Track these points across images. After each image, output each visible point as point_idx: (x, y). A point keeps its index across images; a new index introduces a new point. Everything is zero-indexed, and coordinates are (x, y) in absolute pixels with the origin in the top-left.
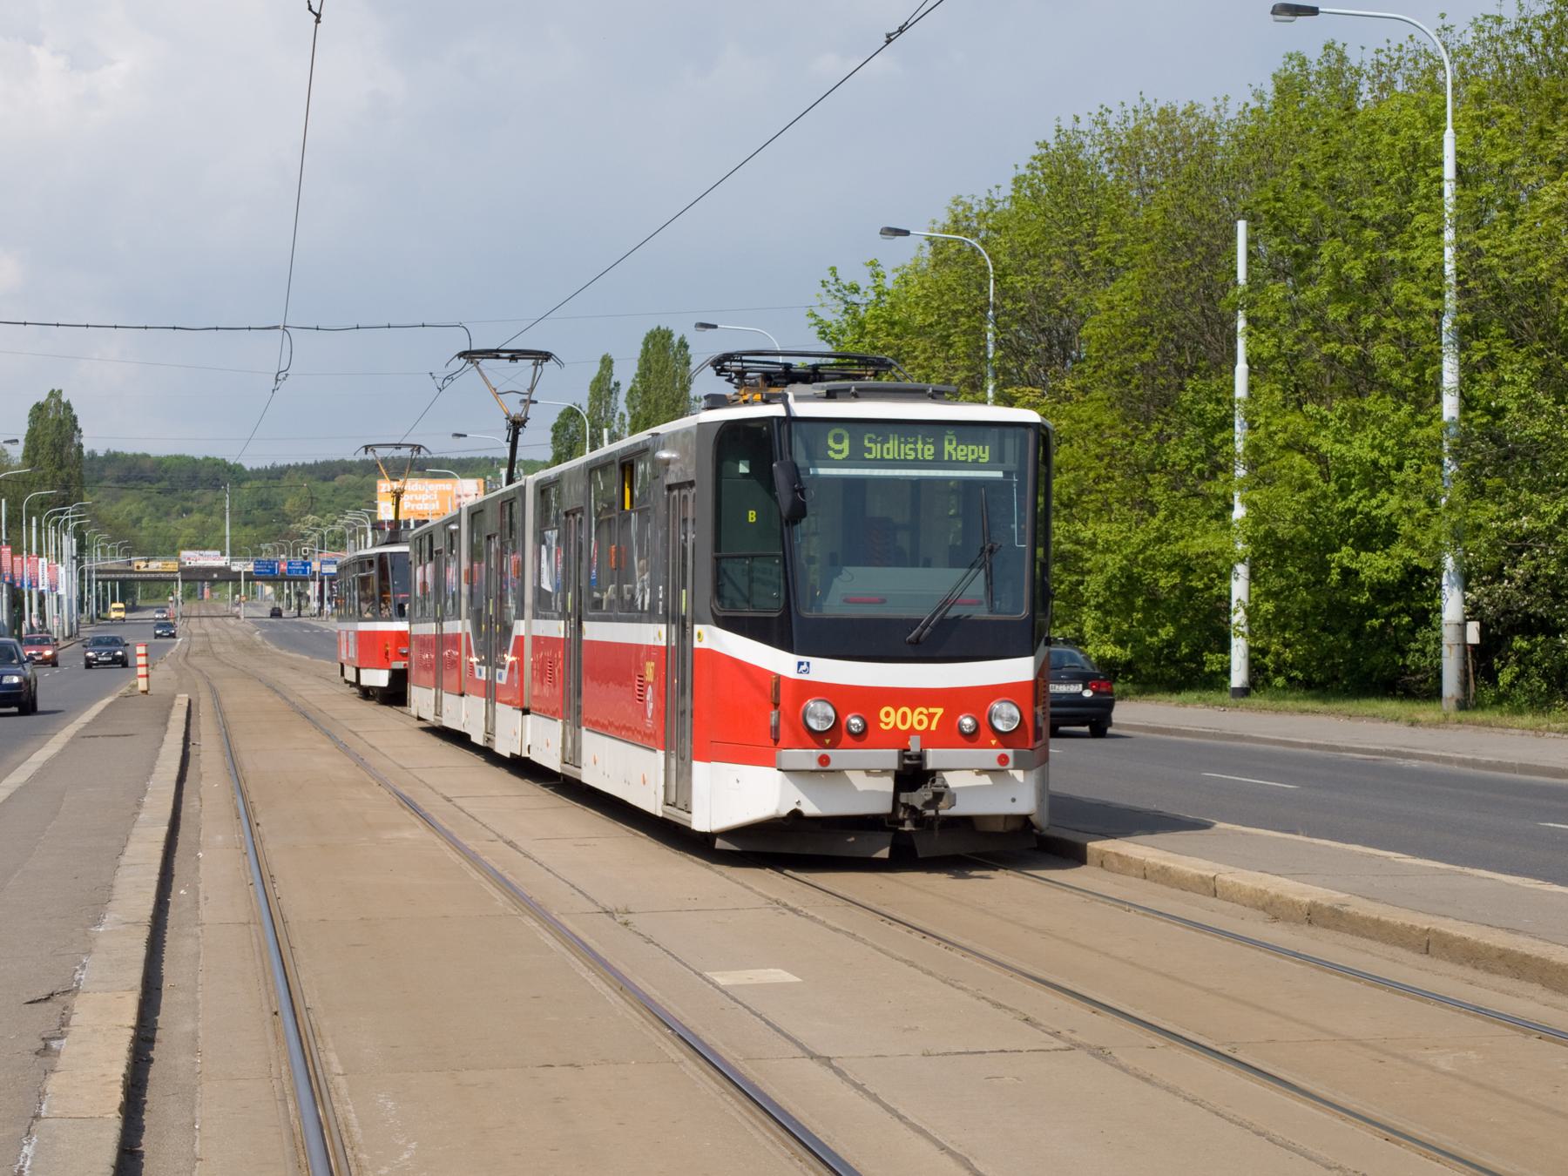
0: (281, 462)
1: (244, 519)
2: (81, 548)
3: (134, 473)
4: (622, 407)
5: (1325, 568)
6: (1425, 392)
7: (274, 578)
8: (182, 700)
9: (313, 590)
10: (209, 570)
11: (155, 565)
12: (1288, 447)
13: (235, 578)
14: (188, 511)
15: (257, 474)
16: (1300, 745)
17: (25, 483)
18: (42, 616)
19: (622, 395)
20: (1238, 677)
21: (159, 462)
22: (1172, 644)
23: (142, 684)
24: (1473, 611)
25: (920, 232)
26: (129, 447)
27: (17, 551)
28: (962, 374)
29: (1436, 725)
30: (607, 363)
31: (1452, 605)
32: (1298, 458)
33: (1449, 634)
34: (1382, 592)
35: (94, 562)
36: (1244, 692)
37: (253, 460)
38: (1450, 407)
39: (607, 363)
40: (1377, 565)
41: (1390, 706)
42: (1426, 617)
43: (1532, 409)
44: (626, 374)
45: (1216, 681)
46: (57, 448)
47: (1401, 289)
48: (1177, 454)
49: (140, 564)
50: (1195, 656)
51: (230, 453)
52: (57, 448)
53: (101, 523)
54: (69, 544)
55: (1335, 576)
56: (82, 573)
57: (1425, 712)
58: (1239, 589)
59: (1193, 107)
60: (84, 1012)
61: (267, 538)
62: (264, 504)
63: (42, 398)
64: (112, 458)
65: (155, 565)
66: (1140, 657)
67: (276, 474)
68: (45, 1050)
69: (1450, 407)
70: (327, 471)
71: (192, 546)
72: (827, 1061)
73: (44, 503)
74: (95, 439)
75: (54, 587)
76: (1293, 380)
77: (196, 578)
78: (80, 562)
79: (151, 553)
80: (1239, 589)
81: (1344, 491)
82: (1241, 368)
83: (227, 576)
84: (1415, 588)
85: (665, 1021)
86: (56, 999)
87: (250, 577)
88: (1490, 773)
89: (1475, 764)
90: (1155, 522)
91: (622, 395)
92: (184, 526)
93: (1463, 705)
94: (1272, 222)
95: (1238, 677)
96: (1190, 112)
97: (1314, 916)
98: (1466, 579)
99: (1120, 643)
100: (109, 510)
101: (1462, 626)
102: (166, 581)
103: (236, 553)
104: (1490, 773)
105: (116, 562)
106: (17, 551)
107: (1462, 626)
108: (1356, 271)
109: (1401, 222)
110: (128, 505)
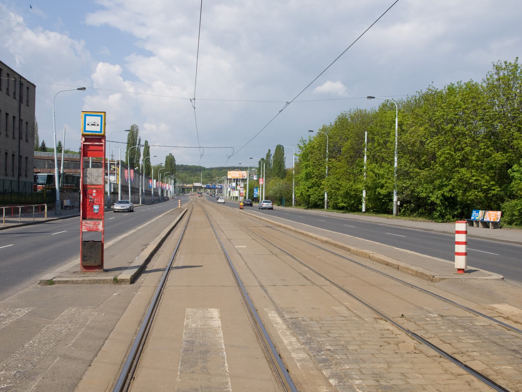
0: (212, 167)
1: (205, 177)
2: (175, 182)
3: (186, 168)
4: (272, 159)
5: (375, 192)
6: (392, 163)
7: (210, 189)
8: (186, 210)
9: (216, 191)
10: (198, 187)
11: (188, 185)
12: (370, 171)
13: (202, 188)
14: (195, 176)
15: (208, 169)
16: (407, 227)
17: (165, 171)
18: (167, 194)
19: (272, 156)
20: (364, 210)
21: (190, 166)
22: (353, 204)
23: (180, 206)
24: (398, 199)
25: (316, 131)
26: (185, 164)
27: (162, 183)
28: (322, 156)
29: (391, 218)
30: (269, 150)
31: (395, 198)
32: (371, 173)
33: (394, 203)
34: (385, 196)
35: (178, 184)
36: (365, 212)
37: (207, 167)
38: (396, 165)
39: (269, 150)
40: (383, 192)
41: (386, 215)
42: (391, 200)
43: (406, 166)
44: (273, 152)
45: (360, 210)
46: (171, 164)
47: (388, 145)
48: (355, 171)
49: (185, 185)
50: (357, 206)
51: (203, 166)
52: (171, 164)
53: (179, 178)
54: (173, 182)
55: (377, 193)
56: (175, 187)
57: (390, 216)
58: (364, 194)
59: (366, 110)
60: (149, 247)
61: (209, 181)
62: (209, 175)
63: (168, 155)
64: (182, 166)
65: (188, 185)
66: (349, 206)
67: (211, 169)
68: (143, 250)
69: (396, 165)
70: (220, 169)
71: (196, 182)
72: (240, 255)
73: (169, 174)
74: (178, 162)
75: (169, 189)
76: (373, 159)
77: (195, 188)
78: (175, 184)
79: (189, 183)
80: (364, 194)
81: (379, 179)
82: (365, 157)
83: (201, 188)
84: (389, 196)
85: (223, 249)
86: (146, 245)
87: (205, 188)
88: (482, 240)
89: (390, 225)
90: (351, 183)
91: (272, 156)
92: (195, 179)
93: (397, 215)
94: (371, 132)
95: (364, 210)
96: (365, 111)
97: (326, 242)
98: (398, 194)
99: (345, 203)
100: (181, 175)
101: (397, 202)
102: (190, 188)
103: (203, 184)
104: (482, 240)
105: (181, 185)
106: (162, 183)
107: (397, 202)
108: (381, 141)
109: (389, 133)
110: (184, 175)
